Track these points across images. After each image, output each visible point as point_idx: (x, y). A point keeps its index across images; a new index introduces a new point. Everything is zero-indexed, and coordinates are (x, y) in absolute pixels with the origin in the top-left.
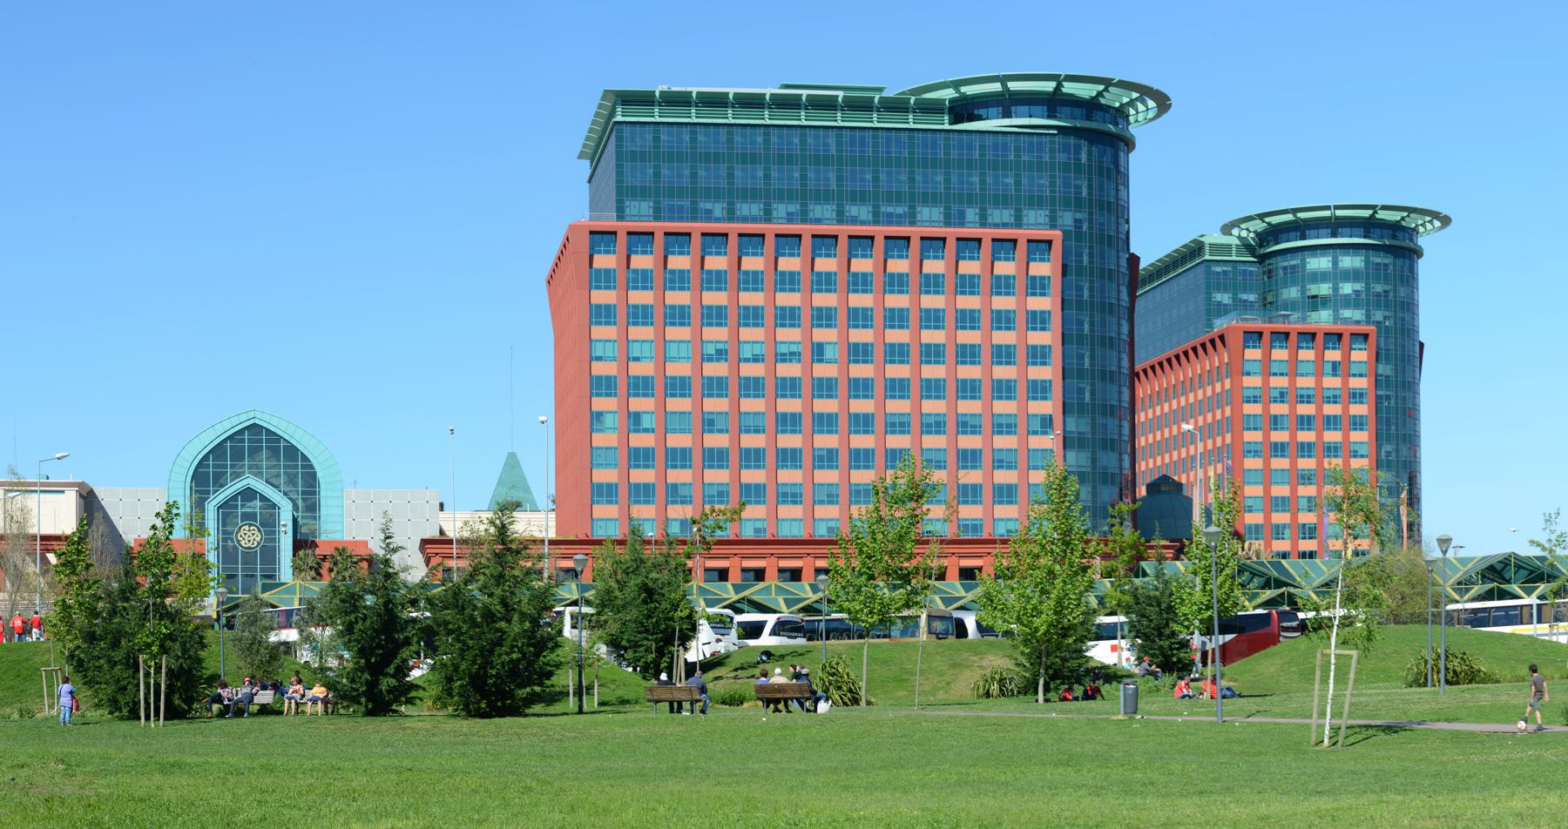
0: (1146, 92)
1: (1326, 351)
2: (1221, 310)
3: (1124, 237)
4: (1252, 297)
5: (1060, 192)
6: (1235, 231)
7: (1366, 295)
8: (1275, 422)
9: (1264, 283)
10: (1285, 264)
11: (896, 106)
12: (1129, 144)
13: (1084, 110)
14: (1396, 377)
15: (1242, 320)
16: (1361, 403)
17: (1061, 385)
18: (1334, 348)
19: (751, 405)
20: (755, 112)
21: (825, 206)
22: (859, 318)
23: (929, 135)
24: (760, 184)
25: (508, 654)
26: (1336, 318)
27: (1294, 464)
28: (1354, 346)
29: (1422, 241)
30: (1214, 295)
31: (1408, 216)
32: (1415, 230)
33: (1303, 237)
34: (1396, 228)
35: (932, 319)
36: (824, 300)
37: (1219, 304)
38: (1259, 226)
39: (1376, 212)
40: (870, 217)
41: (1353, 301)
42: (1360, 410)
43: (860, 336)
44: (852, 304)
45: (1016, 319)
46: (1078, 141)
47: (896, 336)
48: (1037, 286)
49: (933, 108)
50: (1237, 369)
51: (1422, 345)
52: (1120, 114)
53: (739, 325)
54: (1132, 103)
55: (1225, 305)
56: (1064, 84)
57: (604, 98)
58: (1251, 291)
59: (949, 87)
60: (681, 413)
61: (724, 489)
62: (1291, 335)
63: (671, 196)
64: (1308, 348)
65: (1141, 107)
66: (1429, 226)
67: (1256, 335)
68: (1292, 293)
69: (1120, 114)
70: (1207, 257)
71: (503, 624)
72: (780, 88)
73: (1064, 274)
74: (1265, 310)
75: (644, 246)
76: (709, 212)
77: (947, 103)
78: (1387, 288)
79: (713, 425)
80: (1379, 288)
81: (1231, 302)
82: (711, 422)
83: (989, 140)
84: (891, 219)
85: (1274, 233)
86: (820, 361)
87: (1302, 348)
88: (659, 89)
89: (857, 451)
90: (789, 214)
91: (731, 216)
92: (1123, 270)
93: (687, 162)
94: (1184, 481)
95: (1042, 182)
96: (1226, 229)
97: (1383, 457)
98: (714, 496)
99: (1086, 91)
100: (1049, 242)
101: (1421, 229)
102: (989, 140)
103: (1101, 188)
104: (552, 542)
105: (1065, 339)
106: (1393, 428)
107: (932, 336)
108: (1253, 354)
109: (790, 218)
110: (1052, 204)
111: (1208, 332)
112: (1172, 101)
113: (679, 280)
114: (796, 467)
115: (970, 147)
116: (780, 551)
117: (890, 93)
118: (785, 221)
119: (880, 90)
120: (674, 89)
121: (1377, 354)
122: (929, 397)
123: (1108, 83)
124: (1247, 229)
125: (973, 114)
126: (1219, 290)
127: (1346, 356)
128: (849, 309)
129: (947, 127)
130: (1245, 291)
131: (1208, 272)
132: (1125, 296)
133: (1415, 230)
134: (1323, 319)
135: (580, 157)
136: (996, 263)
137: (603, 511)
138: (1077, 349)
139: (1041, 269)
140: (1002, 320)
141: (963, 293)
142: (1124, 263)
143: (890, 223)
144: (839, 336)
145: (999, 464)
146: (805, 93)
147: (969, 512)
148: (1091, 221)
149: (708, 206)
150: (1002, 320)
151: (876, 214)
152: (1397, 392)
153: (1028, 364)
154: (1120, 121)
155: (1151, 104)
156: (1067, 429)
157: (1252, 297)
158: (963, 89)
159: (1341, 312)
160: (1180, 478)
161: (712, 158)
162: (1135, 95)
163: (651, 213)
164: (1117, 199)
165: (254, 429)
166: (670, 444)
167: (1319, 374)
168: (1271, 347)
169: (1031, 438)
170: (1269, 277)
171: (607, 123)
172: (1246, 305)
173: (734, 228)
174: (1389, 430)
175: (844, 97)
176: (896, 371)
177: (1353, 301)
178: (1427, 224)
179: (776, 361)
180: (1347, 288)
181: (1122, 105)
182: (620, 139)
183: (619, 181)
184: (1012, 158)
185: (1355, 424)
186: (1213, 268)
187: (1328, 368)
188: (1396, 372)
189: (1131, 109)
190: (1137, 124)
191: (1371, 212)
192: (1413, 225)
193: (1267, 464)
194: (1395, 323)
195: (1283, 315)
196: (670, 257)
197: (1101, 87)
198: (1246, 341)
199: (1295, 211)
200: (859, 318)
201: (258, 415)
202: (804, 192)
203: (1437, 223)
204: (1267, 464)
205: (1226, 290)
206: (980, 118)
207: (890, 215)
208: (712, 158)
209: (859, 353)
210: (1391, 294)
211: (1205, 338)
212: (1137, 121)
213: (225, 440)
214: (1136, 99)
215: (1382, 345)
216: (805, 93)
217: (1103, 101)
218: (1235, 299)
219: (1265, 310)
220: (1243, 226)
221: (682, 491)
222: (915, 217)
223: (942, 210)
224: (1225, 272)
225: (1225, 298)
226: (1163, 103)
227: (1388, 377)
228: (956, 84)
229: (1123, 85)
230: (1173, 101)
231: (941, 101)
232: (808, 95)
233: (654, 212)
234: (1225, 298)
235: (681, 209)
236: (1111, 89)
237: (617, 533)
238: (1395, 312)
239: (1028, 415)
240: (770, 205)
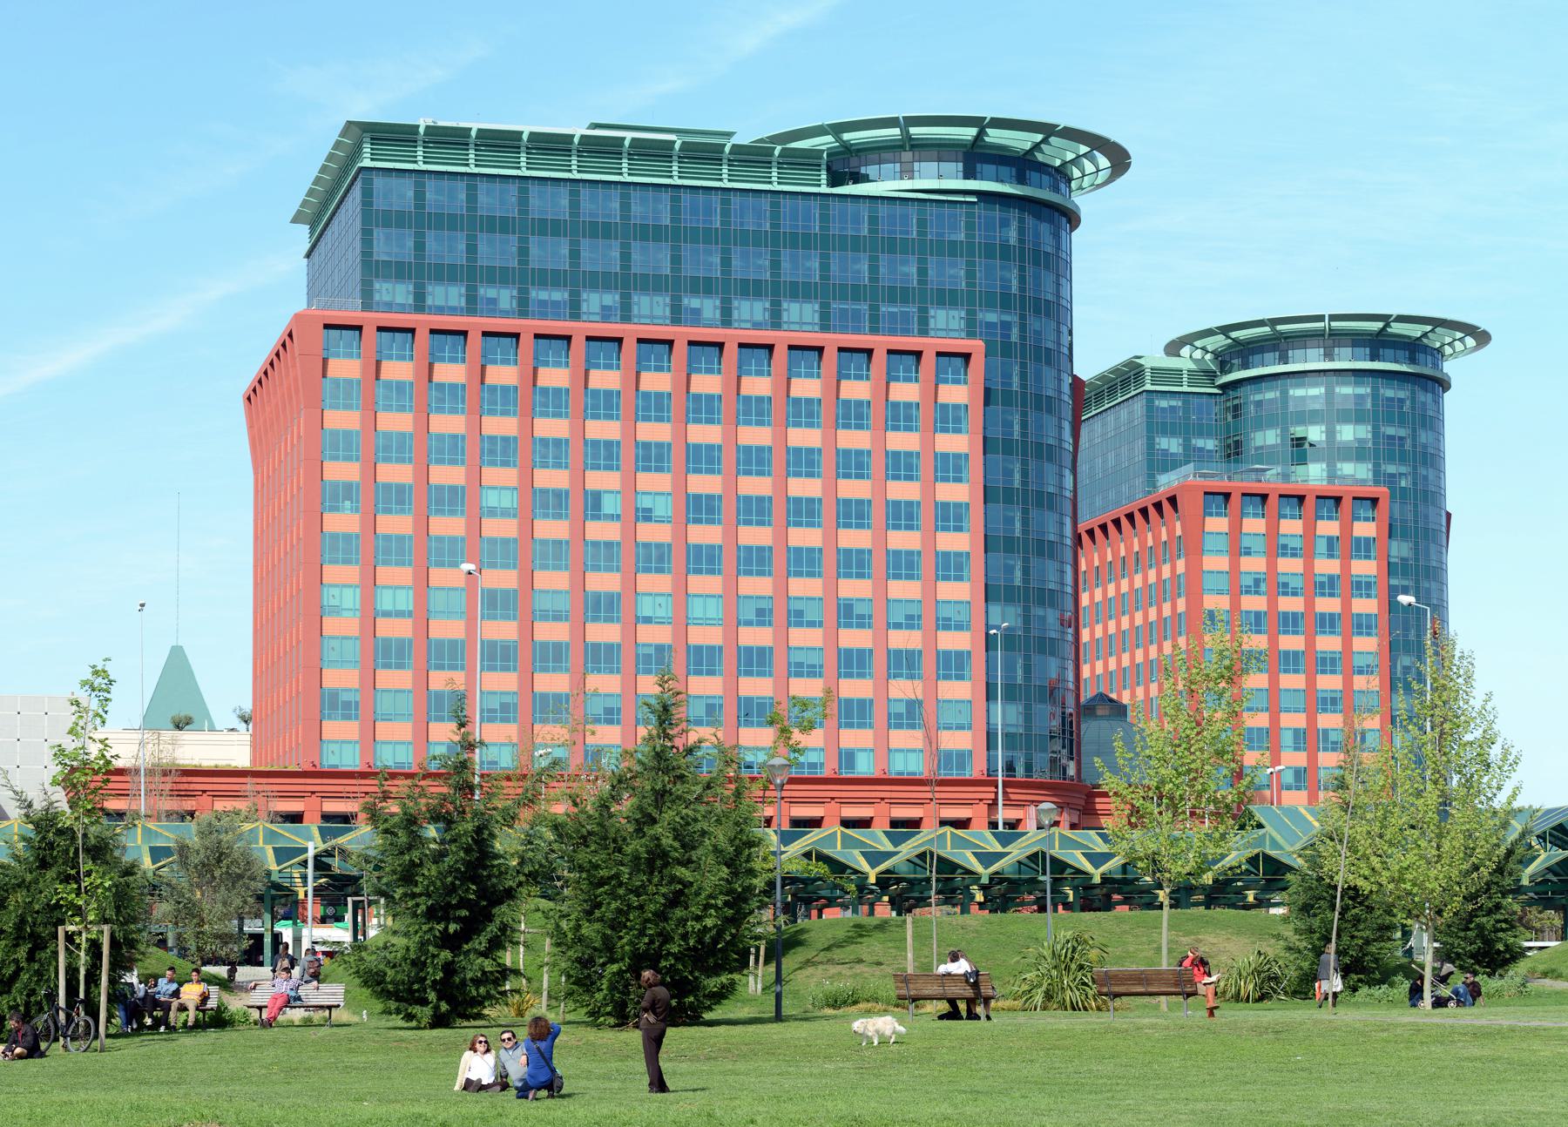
0: (1099, 143)
2: (1168, 463)
4: (1210, 444)
6: (1186, 351)
7: (1374, 444)
8: (847, 614)
9: (1228, 425)
10: (1258, 397)
11: (754, 157)
14: (1417, 560)
15: (1203, 476)
16: (1368, 596)
17: (983, 561)
22: (702, 459)
23: (800, 201)
24: (461, 259)
29: (1449, 368)
30: (1157, 440)
32: (1439, 351)
33: (1284, 359)
35: (804, 462)
36: (902, 441)
37: (1165, 452)
38: (1219, 341)
39: (1387, 325)
40: (463, 303)
41: (1357, 453)
42: (1366, 606)
43: (704, 484)
44: (692, 439)
47: (902, 491)
48: (948, 418)
50: (1192, 546)
51: (1449, 516)
52: (1060, 176)
57: (344, 134)
58: (1209, 436)
63: (844, 298)
64: (1293, 517)
66: (1459, 346)
67: (1332, 501)
68: (1270, 437)
69: (1060, 176)
70: (1148, 387)
73: (987, 402)
74: (1229, 462)
75: (659, 359)
76: (697, 312)
79: (764, 610)
81: (1181, 451)
82: (799, 613)
83: (883, 210)
85: (1244, 351)
86: (597, 517)
87: (1285, 517)
90: (604, 308)
91: (523, 309)
92: (1066, 398)
93: (717, 243)
94: (1126, 700)
95: (760, 262)
96: (1173, 348)
98: (495, 711)
99: (1021, 141)
100: (967, 357)
101: (1448, 350)
102: (864, 210)
105: (988, 495)
106: (1413, 632)
108: (1217, 524)
109: (606, 314)
113: (655, 406)
117: (744, 138)
118: (597, 318)
119: (729, 135)
120: (441, 123)
122: (798, 574)
123: (1048, 130)
124: (1203, 349)
125: (858, 173)
126: (1164, 433)
127: (1347, 529)
128: (688, 445)
129: (824, 189)
130: (1201, 435)
131: (1150, 407)
133: (1439, 351)
134: (1314, 474)
135: (294, 221)
136: (941, 387)
137: (336, 729)
138: (1004, 509)
139: (955, 394)
140: (901, 465)
142: (1066, 389)
143: (543, 316)
144: (675, 485)
145: (800, 670)
148: (1023, 328)
149: (491, 293)
150: (901, 465)
152: (1417, 581)
154: (1062, 186)
155: (1104, 162)
159: (1339, 465)
160: (1119, 695)
163: (817, 320)
168: (1243, 515)
170: (1235, 417)
171: (345, 170)
174: (1407, 636)
176: (854, 539)
177: (1357, 453)
178: (1457, 343)
179: (637, 519)
181: (1064, 164)
182: (367, 194)
183: (367, 254)
184: (718, 225)
186: (1157, 402)
187: (1321, 546)
188: (1416, 554)
190: (1080, 192)
192: (1438, 345)
193: (1274, 681)
194: (1415, 484)
195: (1257, 470)
196: (541, 370)
197: (1039, 137)
198: (1206, 506)
199: (1274, 322)
200: (702, 459)
202: (420, 266)
203: (1470, 342)
205: (1173, 434)
206: (865, 179)
207: (543, 303)
209: (700, 508)
210: (1409, 441)
211: (1148, 502)
214: (1084, 155)
215: (1397, 515)
217: (1040, 157)
218: (1187, 446)
219: (1229, 462)
220: (1198, 343)
222: (579, 307)
223: (817, 307)
224: (1172, 408)
225: (1172, 445)
226: (1120, 160)
227: (1407, 560)
228: (837, 129)
230: (1133, 160)
231: (814, 154)
232: (633, 140)
233: (821, 320)
234: (1172, 445)
235: (857, 315)
236: (1053, 140)
237: (357, 762)
238: (1415, 468)
239: (937, 602)
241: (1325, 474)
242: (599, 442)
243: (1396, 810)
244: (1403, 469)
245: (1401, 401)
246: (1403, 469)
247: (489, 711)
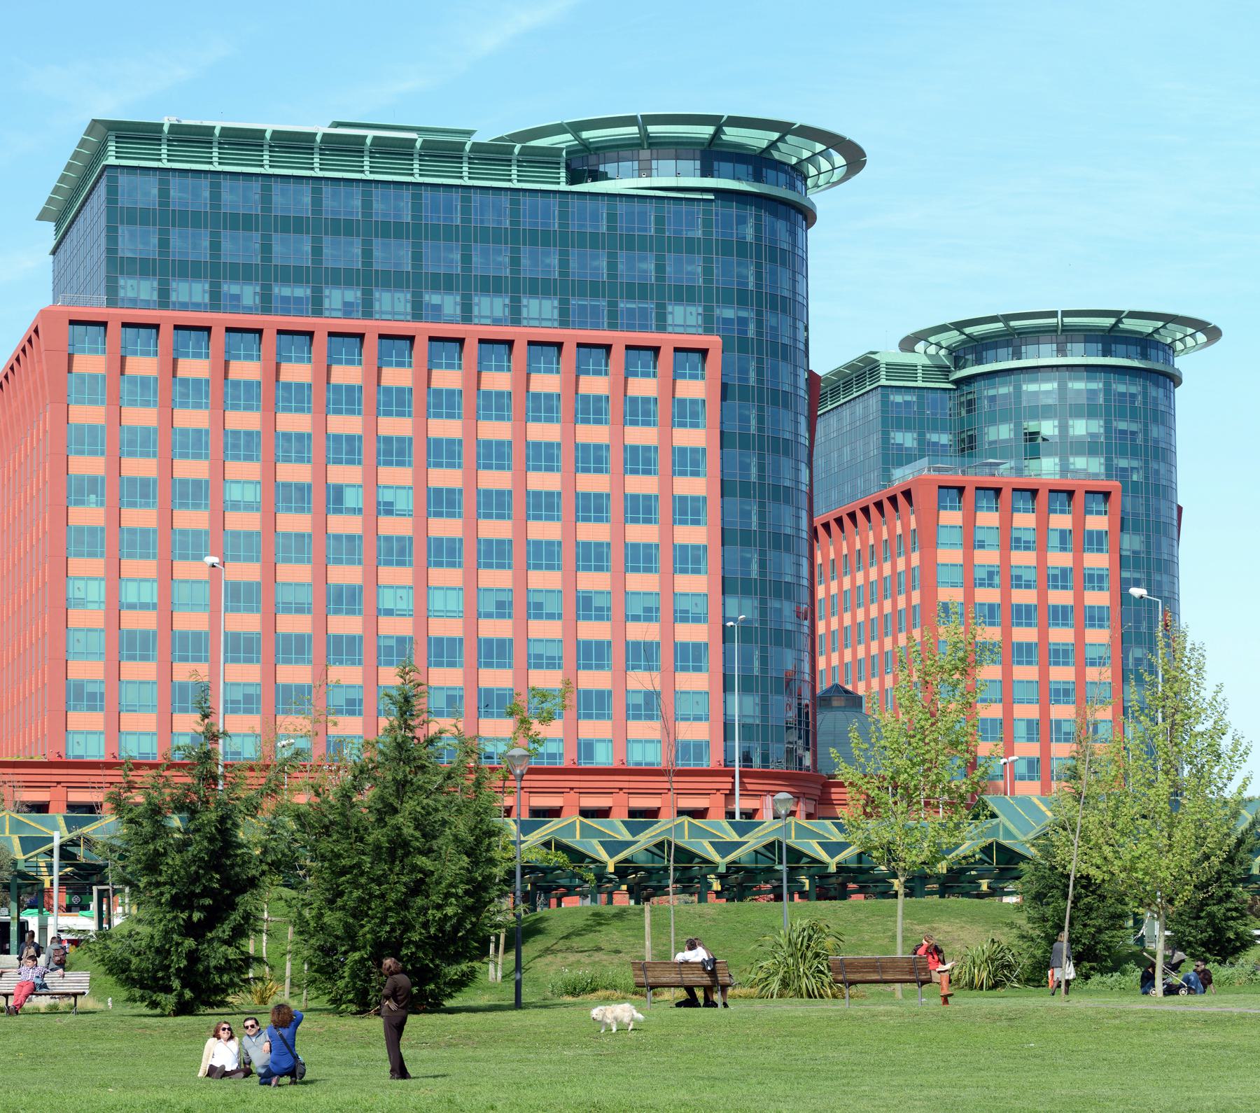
1: (1052, 516)
3: (802, 346)
4: (944, 439)
5: (717, 280)
6: (920, 347)
10: (992, 392)
13: (750, 168)
15: (938, 470)
18: (1062, 512)
19: (542, 580)
20: (301, 157)
21: (397, 295)
22: (442, 453)
23: (540, 199)
25: (439, 907)
26: (1064, 470)
27: (1044, 674)
28: (258, 486)
30: (892, 434)
31: (1163, 327)
32: (1171, 346)
34: (1145, 344)
35: (543, 456)
36: (640, 436)
38: (953, 337)
39: (1119, 321)
40: (207, 300)
41: (1090, 447)
43: (444, 478)
45: (561, 458)
46: (742, 212)
48: (686, 413)
49: (542, 160)
51: (1180, 509)
52: (797, 173)
53: (378, 464)
55: (943, 446)
56: (726, 129)
57: (89, 132)
59: (565, 132)
60: (296, 585)
61: (457, 693)
62: (1003, 492)
63: (582, 294)
64: (1026, 511)
65: (825, 165)
66: (1190, 341)
69: (797, 173)
70: (883, 382)
71: (422, 861)
72: (330, 127)
73: (724, 397)
76: (237, 298)
77: (564, 153)
78: (1134, 427)
83: (621, 207)
84: (288, 306)
85: (977, 347)
86: (338, 511)
87: (1018, 510)
89: (587, 644)
91: (266, 304)
92: (802, 393)
94: (861, 691)
96: (908, 344)
97: (1131, 666)
99: (758, 139)
100: (704, 352)
101: (1179, 346)
102: (603, 207)
106: (1144, 624)
107: (542, 481)
108: (952, 517)
109: (348, 310)
110: (703, 295)
111: (885, 486)
112: (867, 158)
114: (353, 663)
115: (595, 217)
117: (483, 137)
118: (339, 314)
119: (469, 133)
120: (184, 122)
121: (1122, 519)
123: (785, 129)
124: (938, 344)
126: (899, 427)
127: (1079, 523)
129: (563, 187)
131: (885, 402)
132: (803, 430)
133: (1171, 346)
134: (1047, 469)
135: (41, 217)
136: (631, 379)
139: (693, 389)
140: (639, 460)
141: (634, 423)
143: (286, 312)
146: (371, 134)
148: (759, 324)
150: (639, 460)
151: (215, 295)
153: (674, 522)
154: (798, 184)
155: (839, 160)
156: (727, 615)
157: (944, 439)
158: (585, 135)
160: (855, 686)
161: (342, 227)
164: (795, 293)
166: (332, 630)
167: (1041, 547)
168: (976, 508)
169: (631, 625)
170: (969, 412)
171: (90, 167)
172: (935, 450)
173: (271, 322)
175: (424, 141)
177: (1090, 447)
178: (1188, 339)
179: (379, 513)
180: (1080, 428)
181: (800, 162)
182: (112, 191)
183: (111, 251)
185: (1092, 618)
186: (892, 397)
187: (1054, 539)
190: (816, 190)
191: (1112, 321)
192: (1169, 340)
193: (1007, 673)
194: (1146, 478)
195: (991, 464)
197: (775, 136)
199: (1007, 318)
200: (442, 453)
203: (1201, 338)
204: (1007, 673)
205: (908, 428)
206: (604, 177)
207: (285, 300)
208: (342, 227)
209: (442, 502)
210: (1140, 436)
211: (883, 495)
212: (817, 186)
214: (820, 153)
215: (1129, 508)
216: (371, 134)
217: (776, 155)
218: (921, 440)
223: (556, 303)
224: (907, 403)
225: (906, 439)
226: (855, 158)
228: (576, 127)
229: (808, 133)
231: (553, 152)
232: (375, 138)
233: (560, 315)
234: (906, 439)
235: (595, 311)
238: (1146, 462)
240: (370, 293)
241: (1058, 468)
244: (1135, 464)
245: (1133, 396)
246: (1135, 464)
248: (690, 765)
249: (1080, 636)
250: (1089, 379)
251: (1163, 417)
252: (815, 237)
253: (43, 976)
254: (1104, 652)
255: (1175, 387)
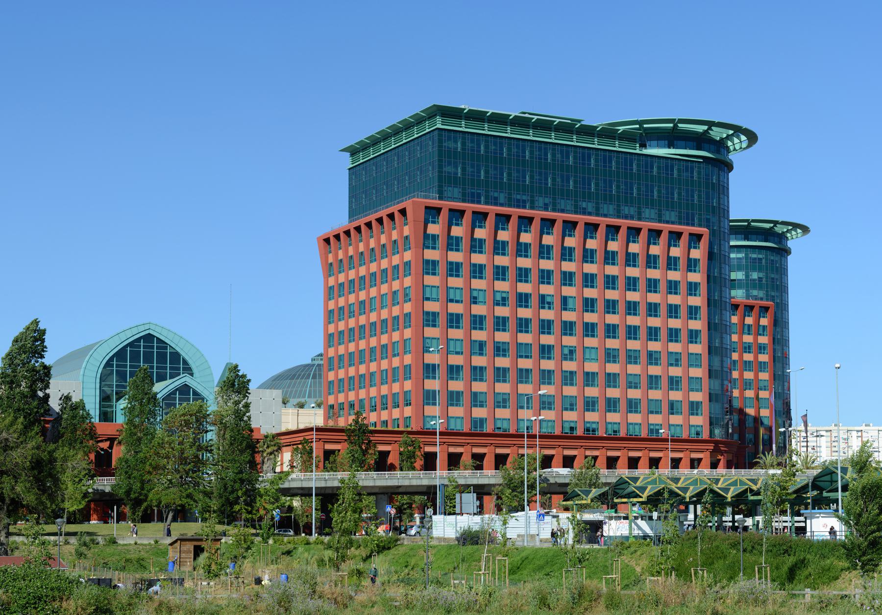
0: (738, 130)
12: (729, 167)
26: (748, 296)
29: (790, 244)
54: (729, 137)
65: (736, 140)
76: (496, 199)
78: (761, 275)
80: (755, 275)
86: (565, 309)
88: (466, 106)
98: (500, 402)
103: (708, 198)
104: (319, 430)
105: (710, 302)
116: (609, 445)
119: (579, 121)
129: (637, 151)
147: (479, 413)
149: (584, 205)
155: (743, 138)
159: (751, 291)
162: (731, 132)
165: (149, 338)
181: (722, 139)
189: (729, 142)
201: (152, 327)
213: (126, 346)
221: (481, 398)
226: (752, 138)
241: (745, 294)
242: (476, 264)
243: (139, 434)
244: (777, 294)
245: (760, 259)
246: (777, 294)
247: (498, 402)
248: (477, 430)
249: (756, 376)
250: (738, 252)
251: (782, 271)
252: (733, 177)
253: (266, 513)
254: (766, 384)
255: (788, 255)
